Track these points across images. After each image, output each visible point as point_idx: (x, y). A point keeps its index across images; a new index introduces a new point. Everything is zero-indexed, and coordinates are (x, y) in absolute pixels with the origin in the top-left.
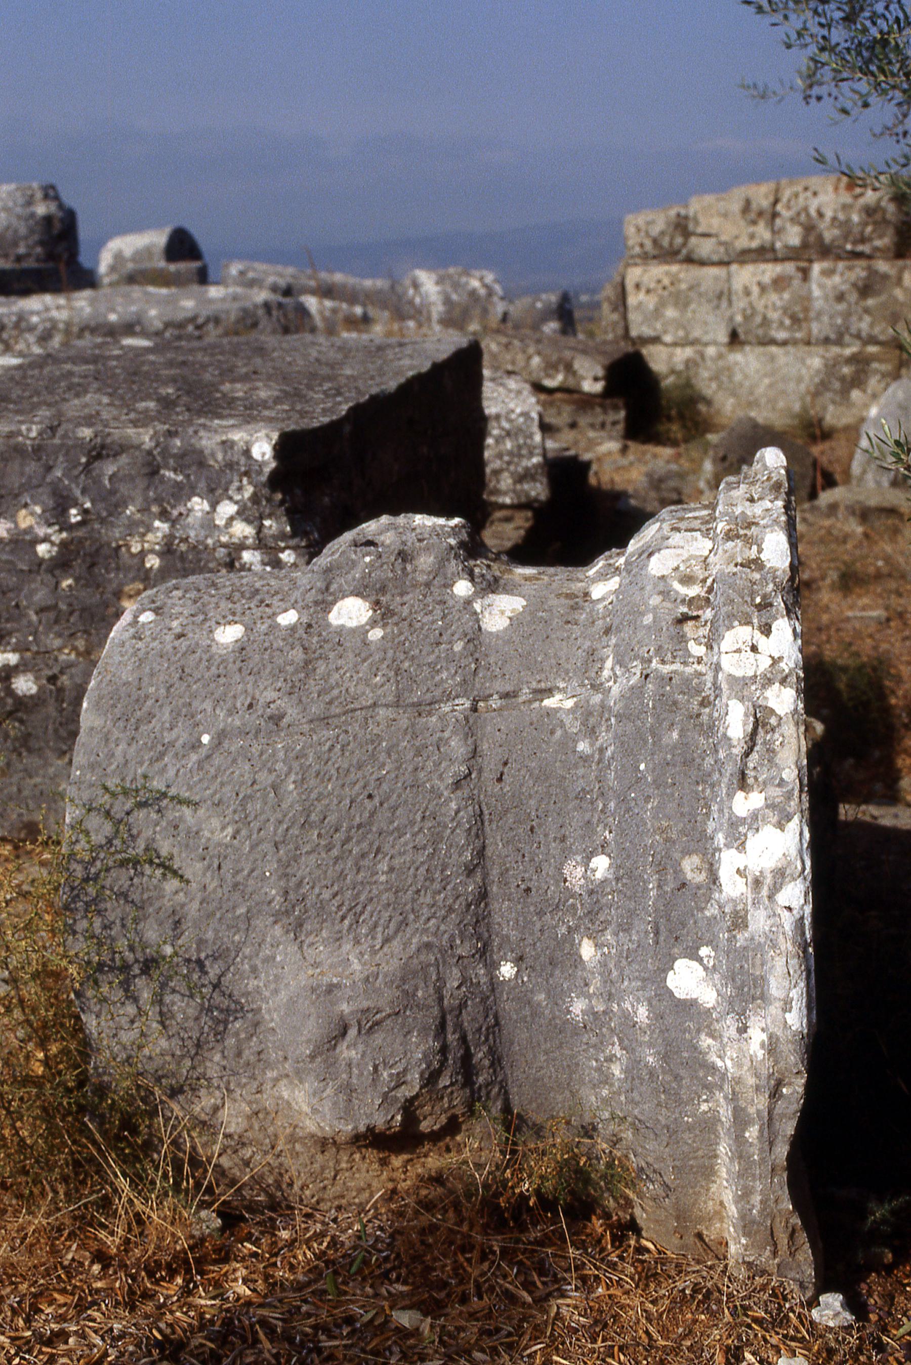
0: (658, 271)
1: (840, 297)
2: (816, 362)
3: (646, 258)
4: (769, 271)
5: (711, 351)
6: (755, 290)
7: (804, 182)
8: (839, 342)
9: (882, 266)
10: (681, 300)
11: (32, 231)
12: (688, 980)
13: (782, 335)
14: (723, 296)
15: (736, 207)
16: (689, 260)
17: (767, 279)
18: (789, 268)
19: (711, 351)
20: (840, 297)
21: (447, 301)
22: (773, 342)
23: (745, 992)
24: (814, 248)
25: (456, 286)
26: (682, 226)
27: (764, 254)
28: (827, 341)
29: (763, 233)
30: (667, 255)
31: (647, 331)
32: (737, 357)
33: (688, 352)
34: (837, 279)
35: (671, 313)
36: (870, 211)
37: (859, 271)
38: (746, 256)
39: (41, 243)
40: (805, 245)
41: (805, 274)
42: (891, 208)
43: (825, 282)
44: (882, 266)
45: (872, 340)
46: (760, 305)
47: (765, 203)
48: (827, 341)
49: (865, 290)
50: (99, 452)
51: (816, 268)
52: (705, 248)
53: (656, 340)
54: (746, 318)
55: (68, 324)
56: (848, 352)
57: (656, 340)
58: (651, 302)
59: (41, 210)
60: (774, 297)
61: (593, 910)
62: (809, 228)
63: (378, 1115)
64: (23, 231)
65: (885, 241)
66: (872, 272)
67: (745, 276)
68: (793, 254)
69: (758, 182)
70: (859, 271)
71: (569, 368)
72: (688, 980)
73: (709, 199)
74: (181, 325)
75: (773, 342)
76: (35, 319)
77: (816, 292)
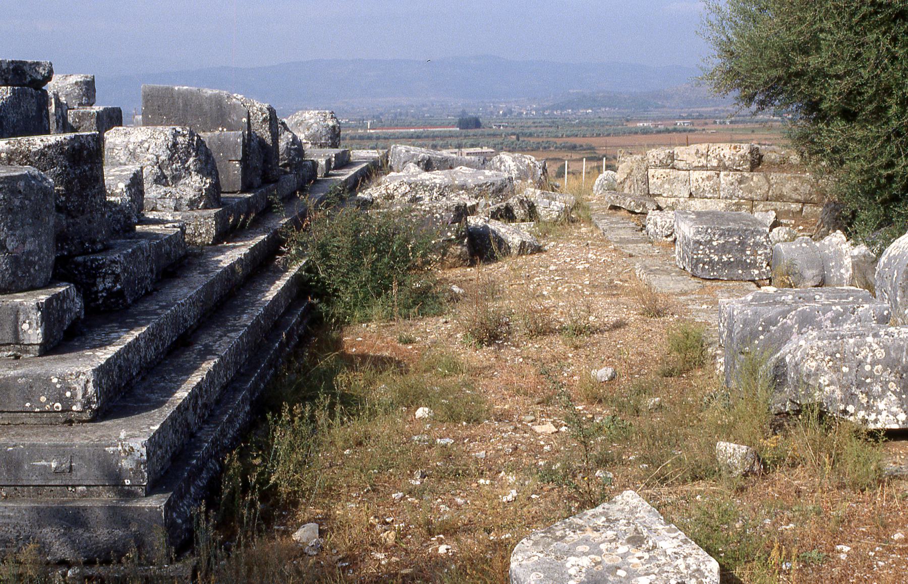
0: (660, 171)
1: (732, 184)
2: (723, 205)
3: (656, 166)
4: (705, 174)
5: (682, 200)
6: (700, 180)
7: (718, 145)
8: (731, 198)
9: (746, 174)
10: (671, 182)
11: (328, 133)
12: (843, 271)
13: (709, 195)
14: (687, 181)
15: (694, 152)
16: (673, 168)
17: (704, 177)
18: (713, 173)
19: (682, 200)
20: (732, 184)
21: (518, 169)
22: (706, 197)
23: (848, 271)
24: (722, 166)
25: (521, 162)
26: (672, 156)
27: (703, 168)
28: (726, 198)
29: (703, 161)
30: (666, 166)
31: (656, 192)
32: (691, 202)
33: (673, 200)
34: (730, 178)
35: (666, 186)
36: (742, 157)
37: (738, 176)
38: (696, 168)
39: (331, 138)
40: (719, 166)
41: (718, 175)
42: (749, 155)
43: (726, 179)
44: (746, 174)
45: (743, 198)
46: (702, 185)
47: (705, 152)
48: (726, 198)
49: (740, 182)
50: (746, 230)
51: (722, 174)
52: (681, 165)
53: (660, 195)
54: (696, 189)
55: (440, 185)
56: (734, 202)
57: (660, 195)
58: (659, 182)
59: (331, 123)
60: (707, 183)
61: (833, 267)
62: (720, 161)
63: (817, 283)
64: (324, 133)
65: (747, 166)
66: (743, 176)
67: (695, 175)
68: (713, 169)
69: (701, 143)
70: (738, 176)
71: (644, 206)
72: (843, 271)
73: (683, 148)
74: (481, 186)
75: (706, 197)
76: (427, 183)
77: (722, 182)
